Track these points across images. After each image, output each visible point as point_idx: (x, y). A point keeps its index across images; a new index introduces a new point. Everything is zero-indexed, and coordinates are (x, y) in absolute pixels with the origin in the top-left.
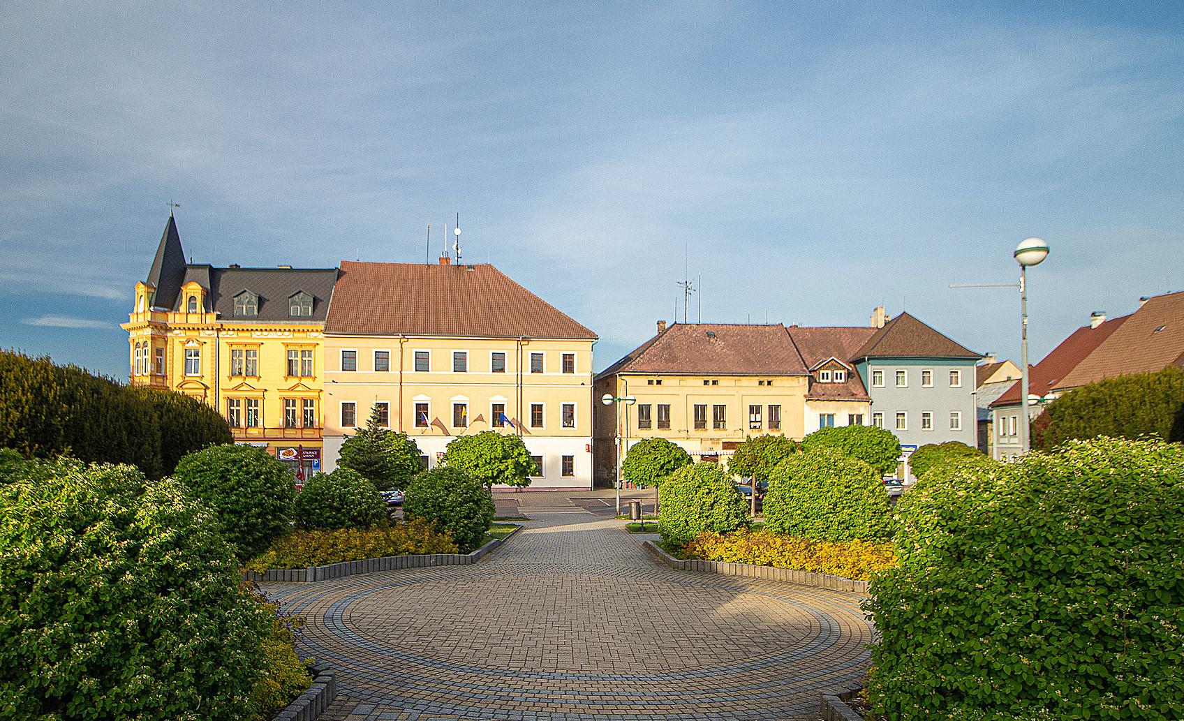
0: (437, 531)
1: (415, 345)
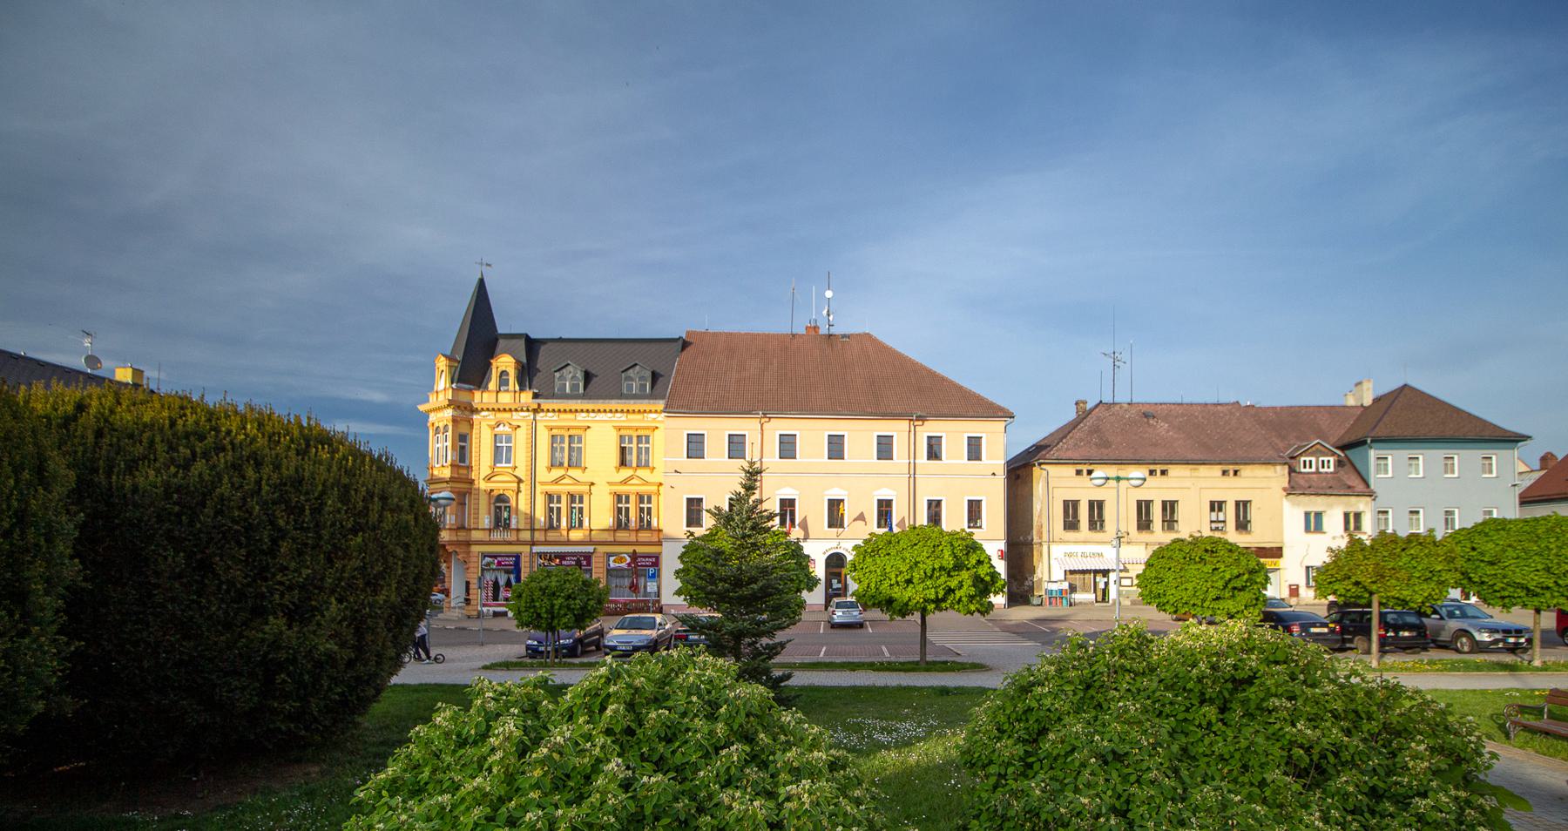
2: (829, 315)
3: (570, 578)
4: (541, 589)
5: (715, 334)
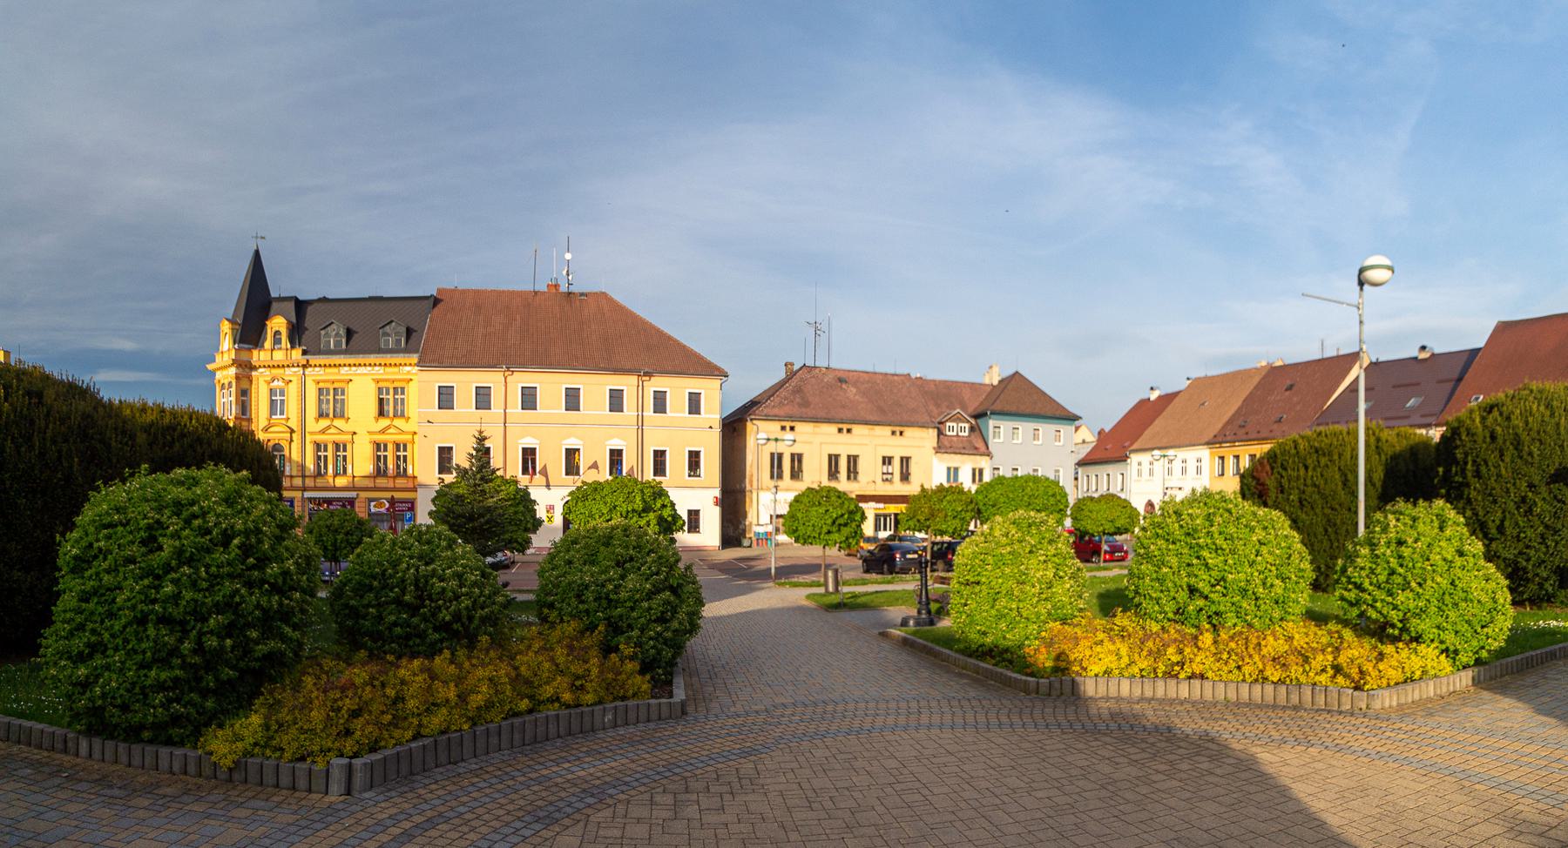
0: (608, 649)
1: (522, 379)
2: (568, 275)
3: (348, 517)
4: (327, 526)
5: (464, 292)
